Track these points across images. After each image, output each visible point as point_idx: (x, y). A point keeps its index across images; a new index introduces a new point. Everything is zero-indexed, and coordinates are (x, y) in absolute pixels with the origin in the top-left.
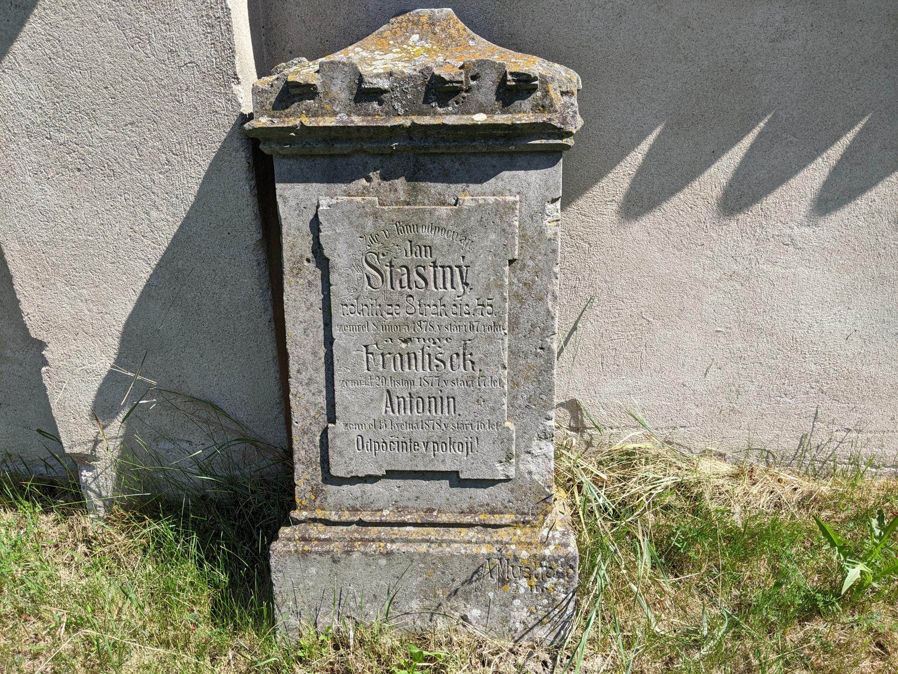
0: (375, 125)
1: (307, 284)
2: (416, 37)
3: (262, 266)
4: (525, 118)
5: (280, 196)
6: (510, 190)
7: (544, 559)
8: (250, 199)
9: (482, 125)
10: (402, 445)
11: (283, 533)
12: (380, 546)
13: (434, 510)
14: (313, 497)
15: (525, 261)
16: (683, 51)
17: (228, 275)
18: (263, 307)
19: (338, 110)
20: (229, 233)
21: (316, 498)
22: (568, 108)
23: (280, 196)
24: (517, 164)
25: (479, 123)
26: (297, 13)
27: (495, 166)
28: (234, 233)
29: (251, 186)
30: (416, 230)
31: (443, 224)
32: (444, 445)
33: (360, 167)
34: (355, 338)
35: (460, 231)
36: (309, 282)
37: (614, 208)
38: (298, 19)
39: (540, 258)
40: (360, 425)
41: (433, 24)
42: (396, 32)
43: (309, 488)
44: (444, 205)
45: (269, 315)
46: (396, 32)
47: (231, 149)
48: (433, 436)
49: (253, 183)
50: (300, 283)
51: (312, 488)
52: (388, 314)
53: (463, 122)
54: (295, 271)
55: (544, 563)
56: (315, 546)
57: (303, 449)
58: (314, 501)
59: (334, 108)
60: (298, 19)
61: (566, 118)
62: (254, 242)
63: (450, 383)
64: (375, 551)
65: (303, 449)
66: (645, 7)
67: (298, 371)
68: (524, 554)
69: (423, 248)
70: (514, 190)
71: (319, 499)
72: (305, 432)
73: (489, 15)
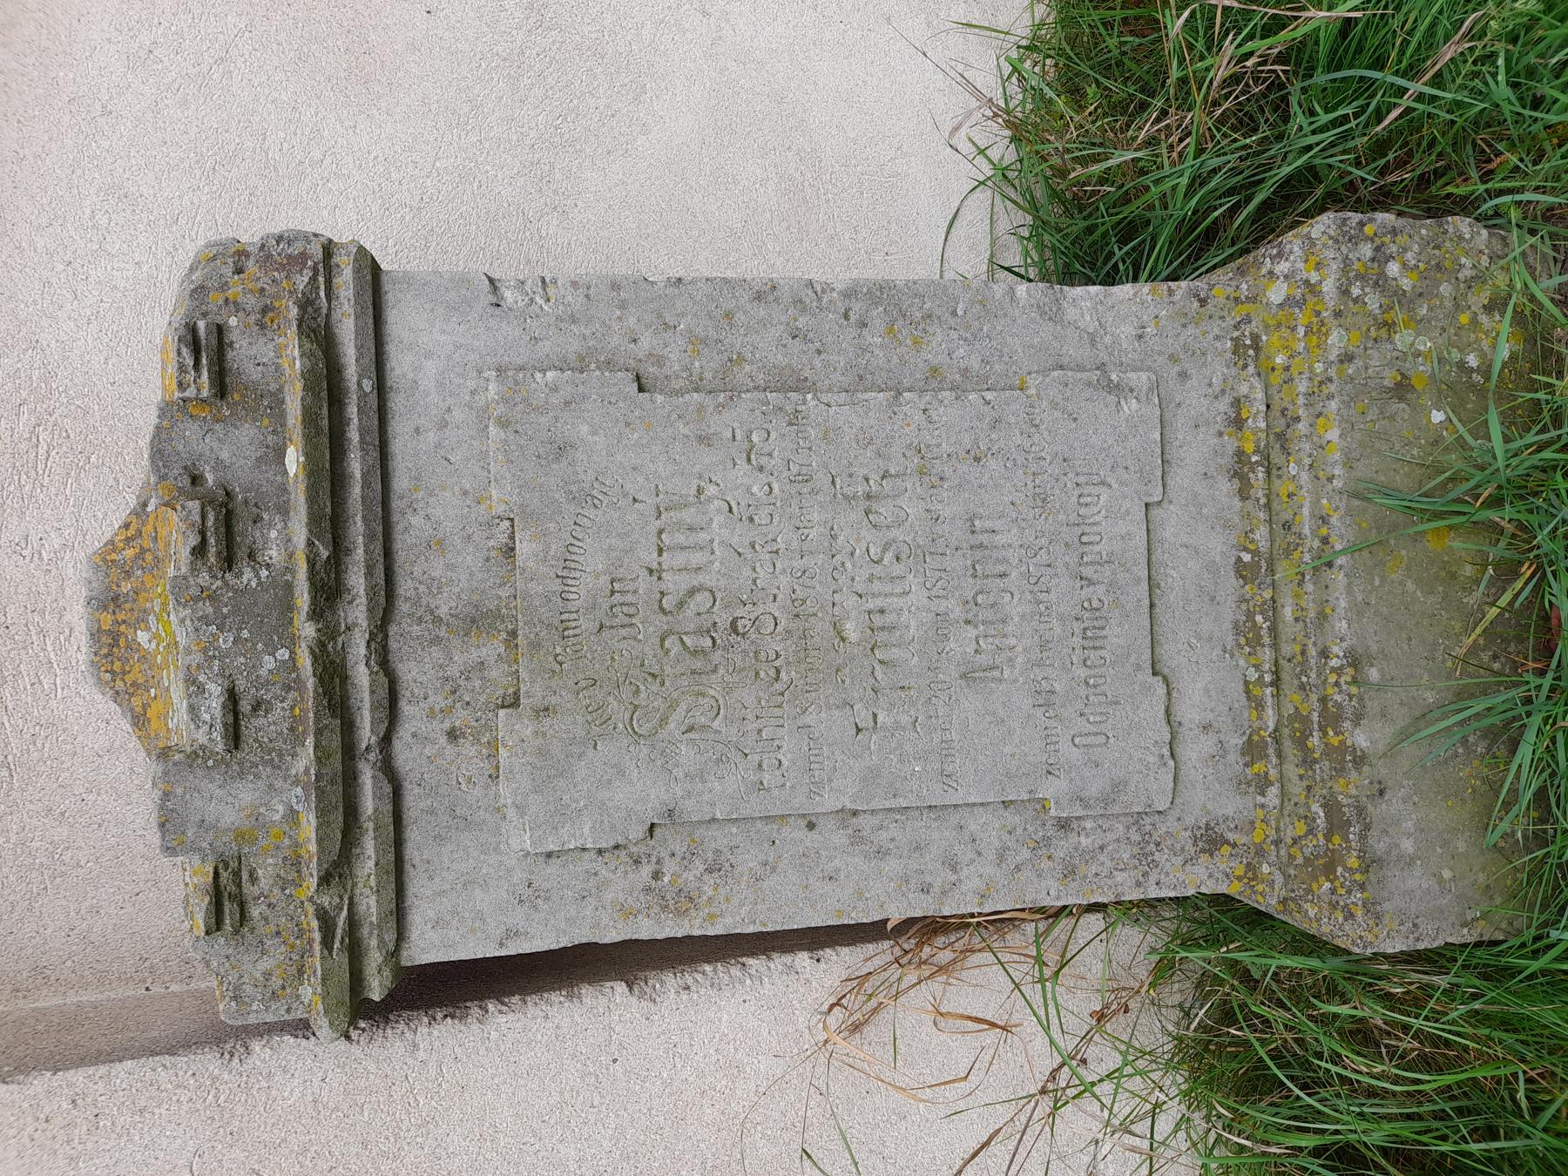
0: (311, 715)
1: (716, 875)
2: (142, 637)
3: (690, 981)
4: (289, 352)
5: (501, 945)
6: (473, 393)
7: (1345, 292)
8: (531, 1010)
9: (307, 455)
10: (1092, 639)
11: (1318, 920)
12: (1337, 684)
13: (1239, 559)
14: (1226, 849)
15: (641, 355)
16: (205, 68)
17: (714, 1059)
18: (784, 977)
19: (281, 808)
20: (615, 1061)
21: (1227, 842)
22: (269, 256)
23: (501, 945)
24: (411, 375)
25: (302, 459)
26: (112, 910)
27: (417, 430)
28: (613, 1048)
29: (501, 1012)
30: (574, 616)
31: (556, 548)
32: (1084, 539)
33: (427, 752)
34: (839, 756)
35: (572, 508)
36: (709, 871)
37: (555, 222)
38: (129, 908)
39: (632, 320)
40: (1049, 740)
41: (115, 599)
42: (134, 684)
43: (1204, 858)
44: (513, 549)
45: (802, 959)
46: (134, 684)
47: (410, 1061)
48: (1067, 565)
49: (491, 1006)
50: (710, 893)
51: (1203, 851)
52: (777, 679)
53: (302, 498)
54: (685, 904)
55: (1356, 291)
56: (1348, 841)
57: (1110, 875)
58: (1234, 845)
59: (277, 817)
60: (129, 908)
61: (289, 257)
62: (634, 1000)
63: (938, 529)
64: (1351, 697)
65: (1110, 875)
66: (106, 144)
67: (925, 889)
68: (1336, 340)
69: (617, 598)
70: (471, 384)
71: (1230, 836)
72: (1069, 873)
73: (122, 481)
